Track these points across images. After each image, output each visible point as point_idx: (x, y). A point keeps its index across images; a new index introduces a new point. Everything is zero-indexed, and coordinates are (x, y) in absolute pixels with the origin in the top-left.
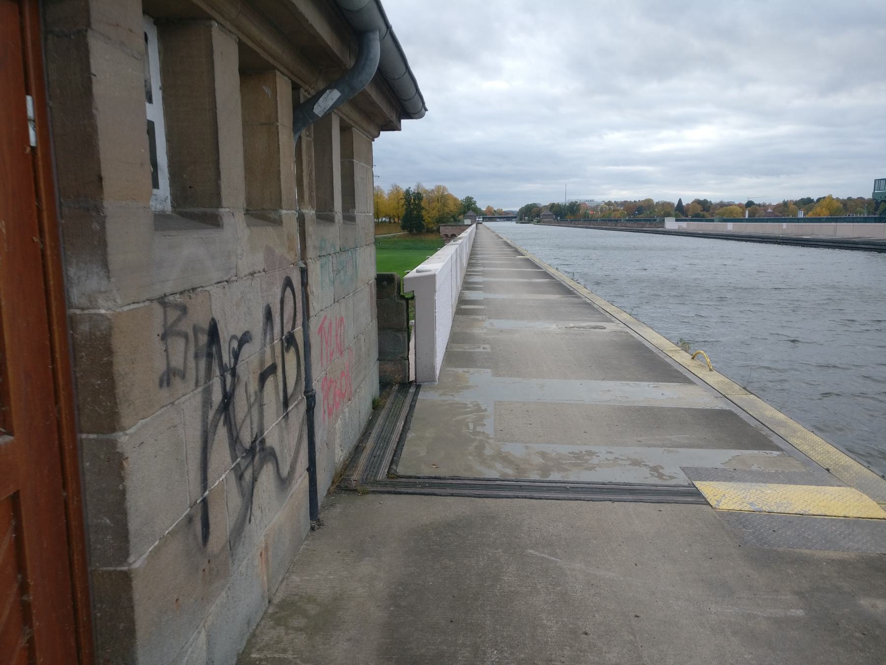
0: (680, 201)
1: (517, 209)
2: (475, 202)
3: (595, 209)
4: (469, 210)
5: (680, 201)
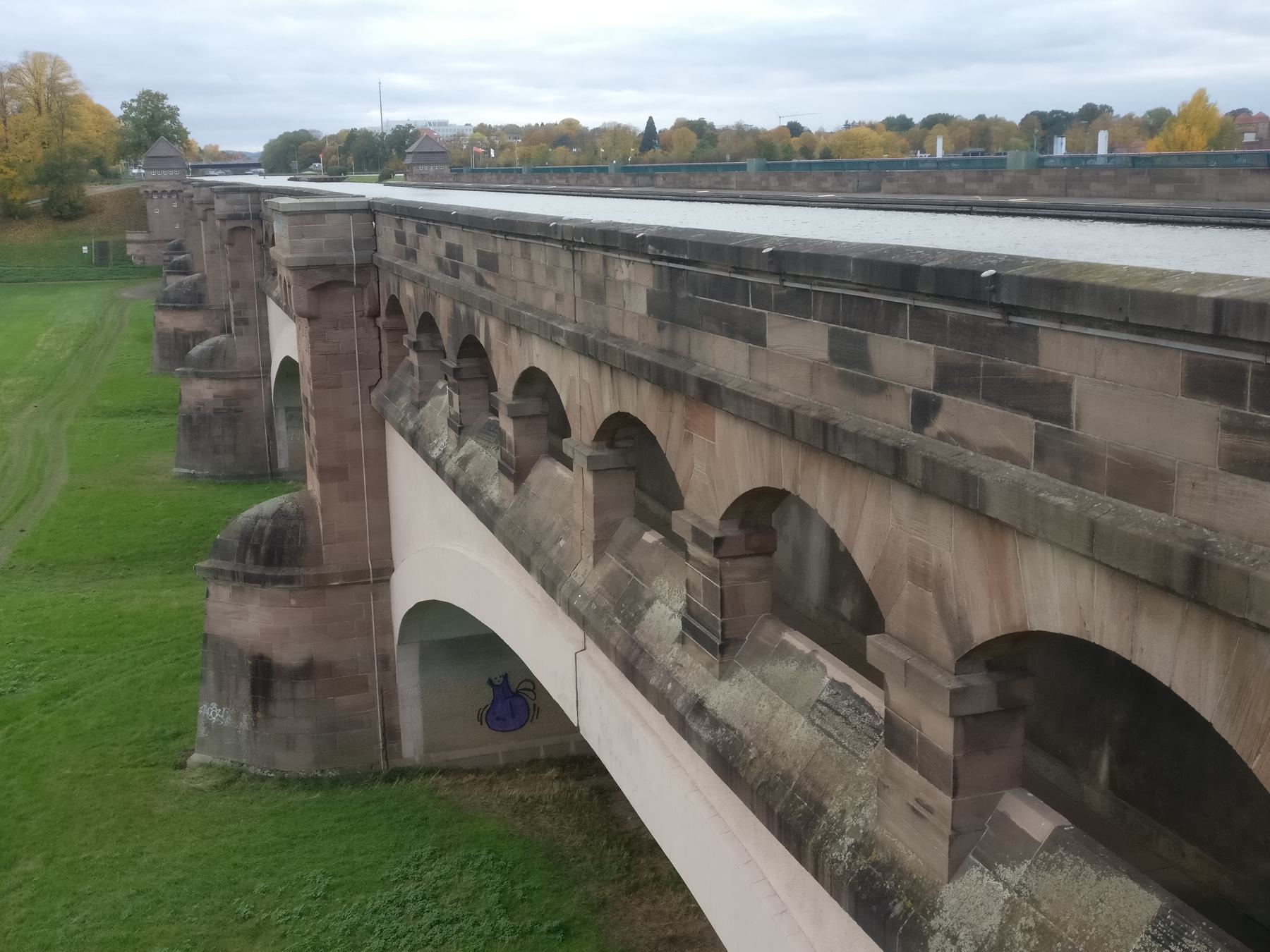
0: (651, 123)
1: (255, 147)
2: (173, 113)
3: (458, 137)
4: (155, 136)
5: (651, 123)
